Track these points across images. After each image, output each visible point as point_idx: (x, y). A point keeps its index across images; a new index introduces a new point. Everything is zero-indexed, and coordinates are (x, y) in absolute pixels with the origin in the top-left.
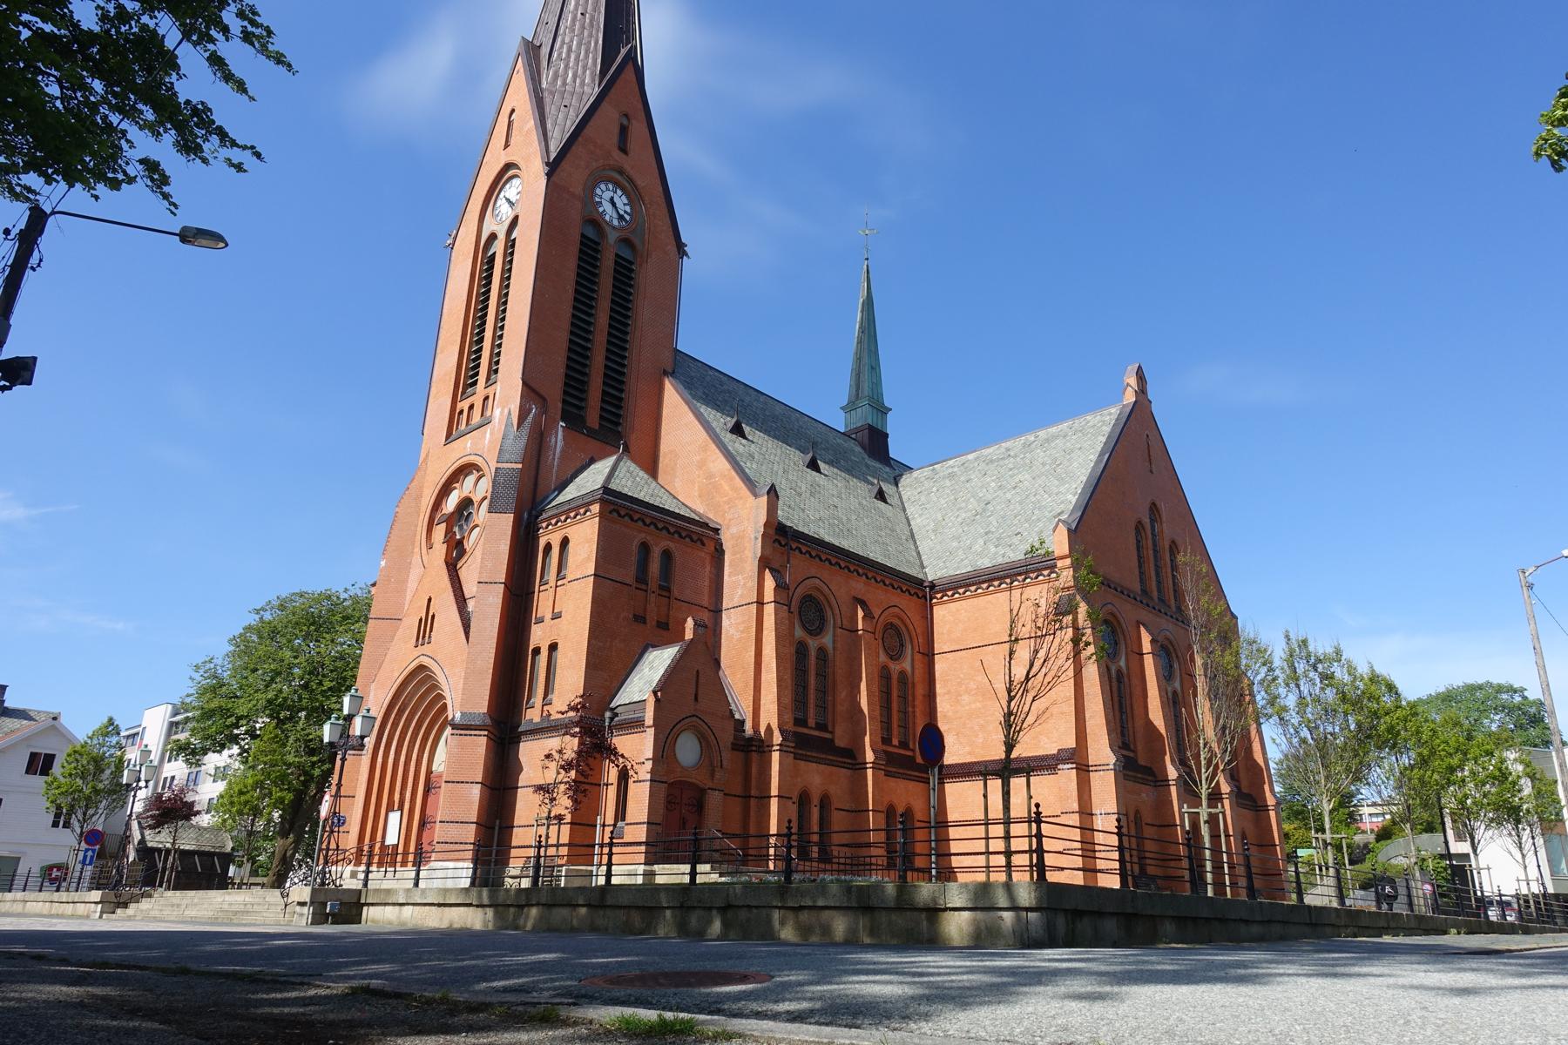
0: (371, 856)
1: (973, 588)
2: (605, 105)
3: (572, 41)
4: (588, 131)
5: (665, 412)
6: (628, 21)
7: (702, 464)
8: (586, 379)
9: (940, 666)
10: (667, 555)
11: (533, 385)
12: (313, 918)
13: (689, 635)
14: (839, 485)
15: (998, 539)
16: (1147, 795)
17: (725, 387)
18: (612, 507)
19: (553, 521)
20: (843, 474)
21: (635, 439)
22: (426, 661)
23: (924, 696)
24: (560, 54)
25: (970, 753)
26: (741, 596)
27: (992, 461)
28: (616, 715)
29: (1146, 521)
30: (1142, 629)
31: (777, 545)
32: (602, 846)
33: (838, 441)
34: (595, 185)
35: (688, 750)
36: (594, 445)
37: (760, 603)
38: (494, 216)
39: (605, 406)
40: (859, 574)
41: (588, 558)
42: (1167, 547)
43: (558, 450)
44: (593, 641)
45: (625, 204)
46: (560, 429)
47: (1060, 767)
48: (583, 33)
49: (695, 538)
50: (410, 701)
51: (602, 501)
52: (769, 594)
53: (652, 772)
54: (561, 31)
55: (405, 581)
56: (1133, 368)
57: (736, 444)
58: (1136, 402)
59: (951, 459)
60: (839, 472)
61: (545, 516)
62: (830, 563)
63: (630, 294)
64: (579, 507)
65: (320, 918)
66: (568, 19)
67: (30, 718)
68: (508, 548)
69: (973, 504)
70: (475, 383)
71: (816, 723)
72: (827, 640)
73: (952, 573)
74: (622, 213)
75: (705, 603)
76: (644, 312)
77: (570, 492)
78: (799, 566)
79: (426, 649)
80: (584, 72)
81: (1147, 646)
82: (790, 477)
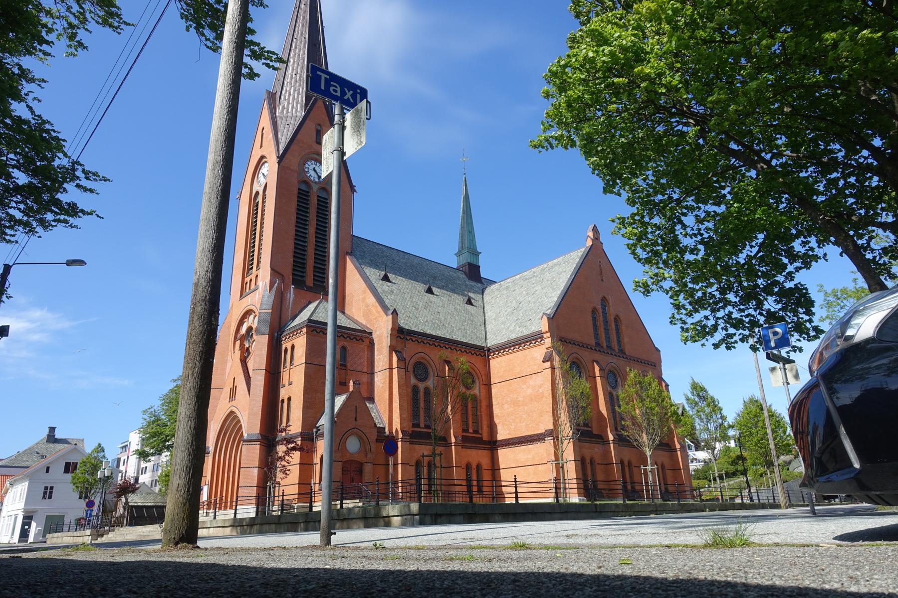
0: (215, 504)
1: (507, 350)
3: (291, 89)
4: (299, 137)
5: (347, 273)
7: (364, 300)
8: (305, 262)
11: (277, 269)
13: (351, 389)
14: (444, 300)
15: (521, 323)
16: (599, 449)
17: (385, 254)
18: (313, 329)
19: (288, 337)
20: (449, 293)
22: (234, 409)
23: (487, 406)
24: (285, 97)
25: (509, 434)
27: (526, 279)
28: (319, 430)
29: (599, 307)
30: (595, 364)
31: (399, 339)
32: (279, 496)
34: (305, 162)
35: (353, 445)
37: (391, 369)
39: (315, 274)
40: (446, 348)
41: (302, 355)
42: (613, 319)
43: (291, 300)
44: (306, 395)
46: (292, 289)
47: (546, 439)
49: (358, 338)
50: (229, 428)
51: (307, 326)
52: (395, 364)
54: (285, 85)
55: (225, 369)
56: (591, 227)
57: (382, 286)
58: (592, 245)
59: (508, 278)
60: (446, 292)
61: (284, 334)
62: (430, 344)
64: (298, 330)
66: (288, 77)
67: (69, 443)
68: (266, 352)
69: (514, 304)
70: (252, 268)
71: (425, 425)
72: (430, 383)
73: (498, 342)
77: (297, 321)
78: (411, 349)
79: (233, 403)
80: (297, 106)
81: (597, 373)
82: (414, 300)
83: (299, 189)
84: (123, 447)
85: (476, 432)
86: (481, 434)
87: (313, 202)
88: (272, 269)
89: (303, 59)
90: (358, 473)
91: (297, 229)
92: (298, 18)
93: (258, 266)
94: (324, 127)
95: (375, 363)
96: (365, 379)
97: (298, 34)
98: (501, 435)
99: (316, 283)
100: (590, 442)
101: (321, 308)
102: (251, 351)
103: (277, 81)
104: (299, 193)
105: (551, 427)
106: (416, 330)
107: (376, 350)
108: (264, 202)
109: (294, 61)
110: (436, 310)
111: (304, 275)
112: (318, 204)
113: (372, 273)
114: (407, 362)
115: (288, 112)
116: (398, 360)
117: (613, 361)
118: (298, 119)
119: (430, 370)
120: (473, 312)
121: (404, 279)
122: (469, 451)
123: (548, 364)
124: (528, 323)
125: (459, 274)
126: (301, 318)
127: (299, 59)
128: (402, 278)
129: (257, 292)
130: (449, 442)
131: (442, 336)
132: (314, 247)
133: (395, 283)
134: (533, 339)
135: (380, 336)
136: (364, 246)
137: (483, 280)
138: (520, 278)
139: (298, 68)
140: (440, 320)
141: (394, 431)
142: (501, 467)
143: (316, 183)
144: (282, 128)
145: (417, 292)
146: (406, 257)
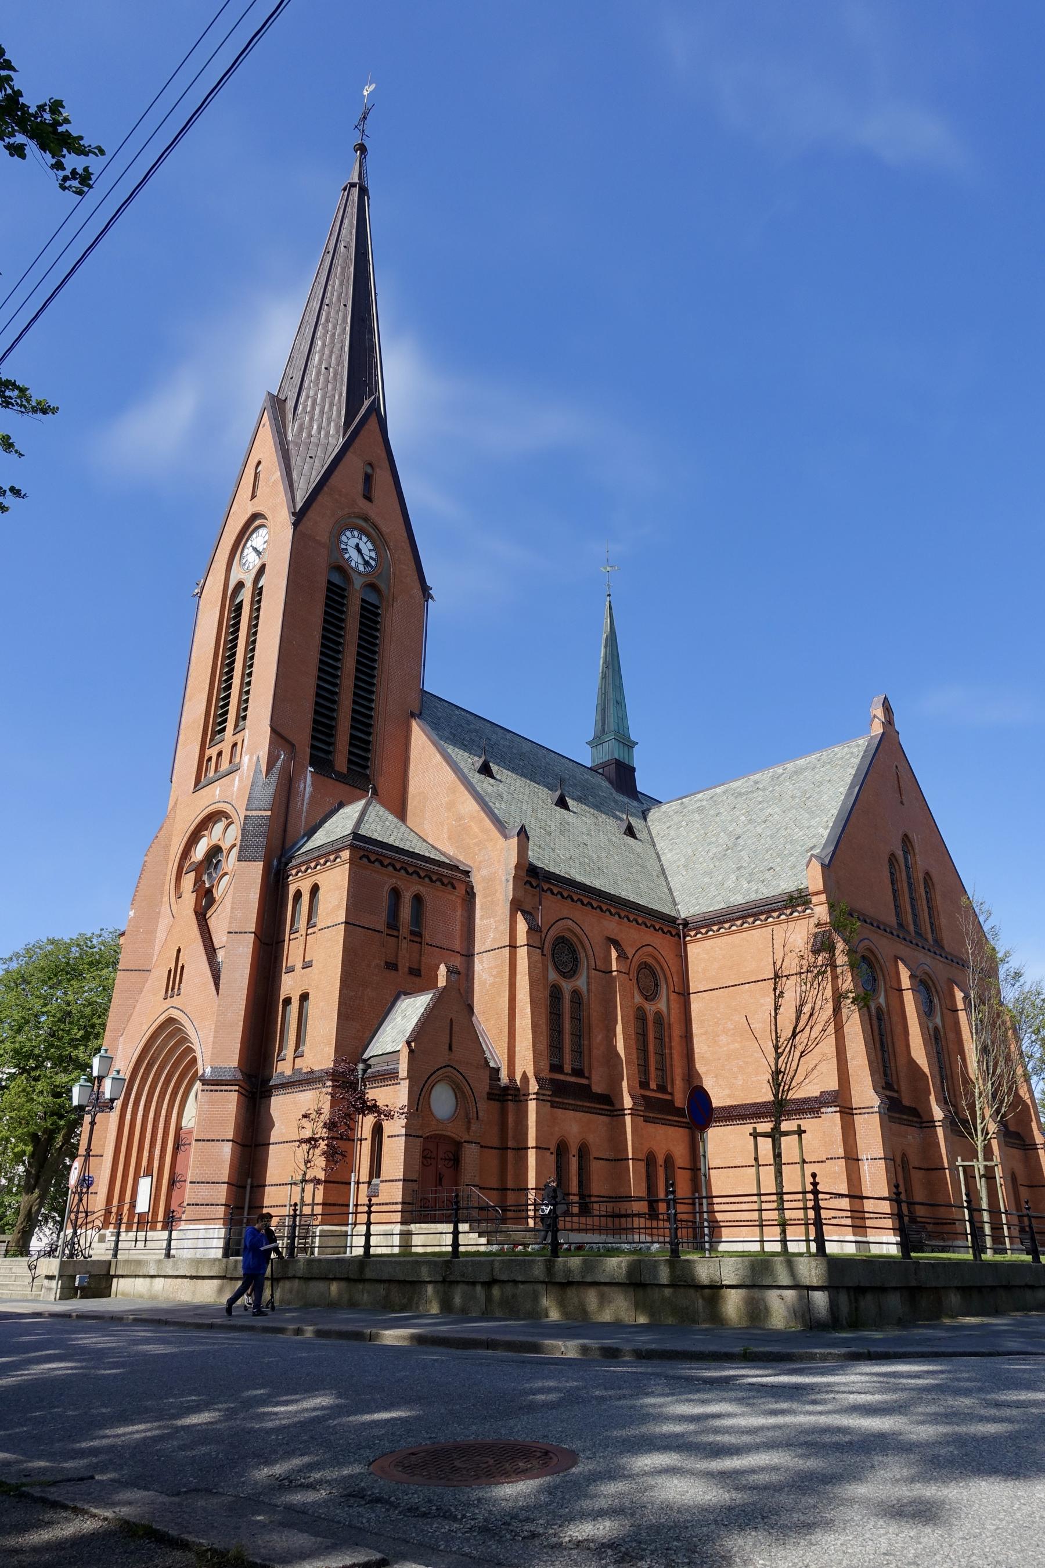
2: (349, 455)
3: (316, 394)
4: (334, 480)
5: (414, 754)
6: (371, 374)
7: (451, 806)
8: (334, 723)
10: (418, 899)
13: (442, 982)
15: (750, 875)
17: (472, 726)
18: (362, 853)
19: (303, 868)
21: (384, 782)
22: (175, 1014)
24: (305, 407)
25: (729, 1096)
26: (494, 940)
27: (740, 794)
28: (369, 1066)
29: (899, 853)
31: (528, 887)
33: (586, 776)
34: (341, 533)
36: (342, 789)
37: (513, 946)
38: (242, 565)
41: (339, 906)
42: (921, 880)
45: (370, 550)
46: (309, 774)
49: (446, 881)
50: (159, 1055)
51: (352, 847)
52: (522, 937)
53: (407, 1126)
54: (306, 385)
57: (484, 784)
58: (883, 734)
59: (699, 793)
61: (294, 863)
63: (376, 638)
65: (68, 1292)
66: (312, 373)
69: (723, 838)
70: (223, 730)
71: (573, 1069)
72: (581, 982)
74: (367, 558)
75: (457, 948)
76: (390, 654)
77: (320, 838)
78: (551, 908)
79: (175, 1001)
81: (906, 982)
82: (539, 816)
85: (662, 1088)
86: (671, 1094)
88: (273, 730)
89: (342, 342)
90: (452, 1162)
94: (378, 470)
97: (332, 296)
102: (215, 895)
103: (287, 381)
105: (833, 1085)
107: (478, 907)
111: (331, 749)
115: (310, 435)
116: (530, 929)
117: (928, 962)
118: (330, 449)
124: (768, 875)
125: (600, 780)
127: (333, 342)
128: (509, 773)
129: (237, 776)
130: (618, 1107)
131: (603, 889)
132: (351, 696)
137: (640, 795)
138: (725, 792)
139: (330, 357)
141: (518, 1078)
143: (360, 573)
144: (299, 461)
145: (540, 803)
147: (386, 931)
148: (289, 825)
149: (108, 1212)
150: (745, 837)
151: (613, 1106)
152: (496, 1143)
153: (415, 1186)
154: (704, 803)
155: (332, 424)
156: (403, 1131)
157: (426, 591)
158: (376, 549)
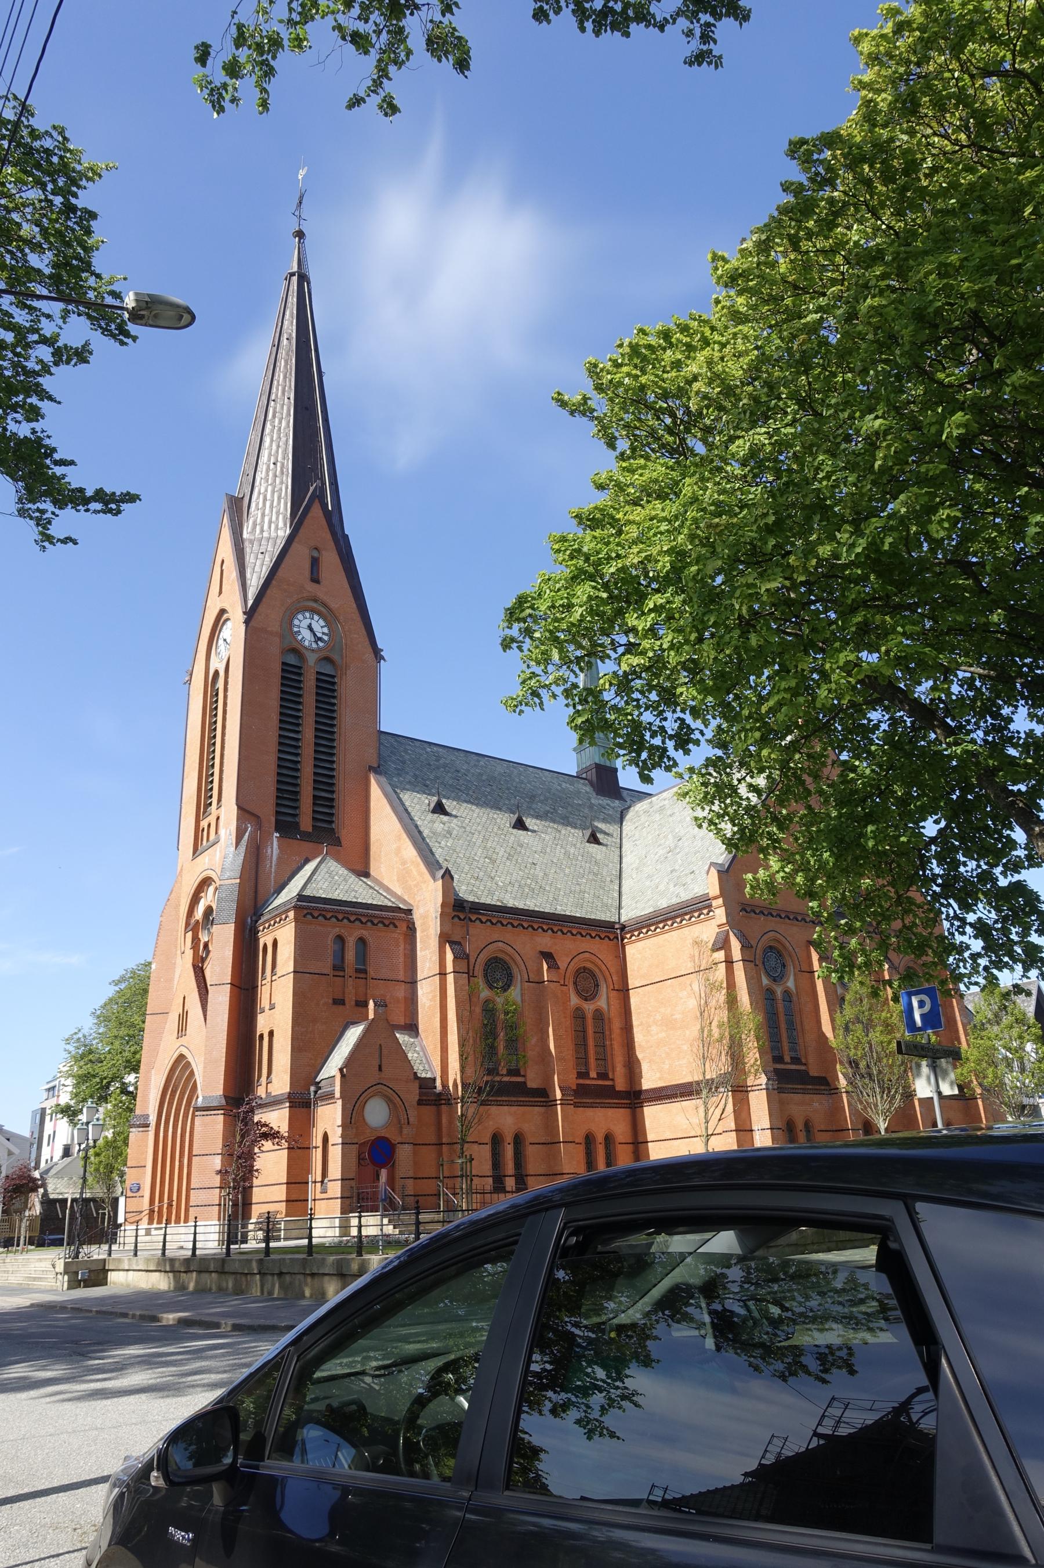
1: (653, 928)
2: (295, 545)
3: (266, 490)
4: (280, 573)
5: (373, 804)
7: (398, 851)
9: (635, 999)
10: (362, 941)
12: (69, 1285)
13: (371, 1016)
15: (679, 877)
18: (305, 912)
20: (556, 826)
21: (347, 834)
22: (185, 1052)
24: (258, 504)
25: (660, 1079)
28: (320, 1088)
31: (456, 920)
33: (564, 785)
35: (377, 1114)
36: (307, 846)
37: (443, 974)
38: (218, 654)
41: (289, 958)
48: (275, 481)
49: (387, 922)
51: (296, 908)
52: (450, 967)
53: (343, 1136)
54: (257, 483)
57: (430, 824)
61: (260, 921)
62: (513, 926)
63: (334, 704)
68: (231, 953)
69: (670, 842)
70: (210, 804)
74: (319, 635)
75: (401, 977)
76: (347, 719)
79: (183, 1040)
80: (277, 518)
83: (283, 664)
84: (49, 1090)
85: (603, 1076)
86: (612, 1080)
87: (309, 683)
89: (287, 435)
91: (282, 733)
92: (278, 364)
93: (219, 800)
95: (419, 964)
96: (401, 992)
97: (277, 391)
98: (649, 1081)
99: (319, 824)
100: (805, 1092)
101: (322, 873)
103: (245, 476)
104: (283, 670)
106: (488, 901)
108: (226, 690)
109: (272, 441)
110: (530, 860)
112: (318, 687)
113: (415, 801)
114: (472, 960)
118: (279, 541)
119: (515, 971)
120: (598, 857)
121: (474, 807)
122: (590, 1112)
123: (720, 955)
124: (689, 880)
126: (290, 891)
129: (218, 846)
132: (312, 762)
133: (456, 817)
134: (698, 907)
135: (425, 917)
136: (406, 751)
137: (625, 793)
139: (277, 452)
140: (535, 879)
142: (650, 1138)
144: (252, 560)
145: (495, 830)
146: (482, 763)
147: (332, 973)
148: (259, 886)
149: (152, 1211)
150: (684, 839)
151: (548, 1097)
152: (432, 1139)
153: (353, 1183)
154: (666, 802)
155: (281, 517)
156: (340, 1141)
157: (377, 654)
158: (328, 624)
